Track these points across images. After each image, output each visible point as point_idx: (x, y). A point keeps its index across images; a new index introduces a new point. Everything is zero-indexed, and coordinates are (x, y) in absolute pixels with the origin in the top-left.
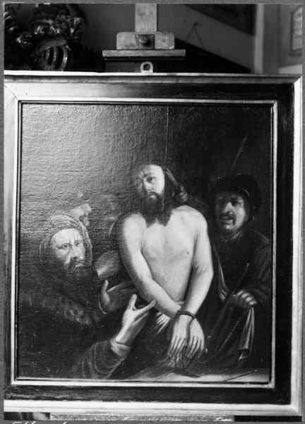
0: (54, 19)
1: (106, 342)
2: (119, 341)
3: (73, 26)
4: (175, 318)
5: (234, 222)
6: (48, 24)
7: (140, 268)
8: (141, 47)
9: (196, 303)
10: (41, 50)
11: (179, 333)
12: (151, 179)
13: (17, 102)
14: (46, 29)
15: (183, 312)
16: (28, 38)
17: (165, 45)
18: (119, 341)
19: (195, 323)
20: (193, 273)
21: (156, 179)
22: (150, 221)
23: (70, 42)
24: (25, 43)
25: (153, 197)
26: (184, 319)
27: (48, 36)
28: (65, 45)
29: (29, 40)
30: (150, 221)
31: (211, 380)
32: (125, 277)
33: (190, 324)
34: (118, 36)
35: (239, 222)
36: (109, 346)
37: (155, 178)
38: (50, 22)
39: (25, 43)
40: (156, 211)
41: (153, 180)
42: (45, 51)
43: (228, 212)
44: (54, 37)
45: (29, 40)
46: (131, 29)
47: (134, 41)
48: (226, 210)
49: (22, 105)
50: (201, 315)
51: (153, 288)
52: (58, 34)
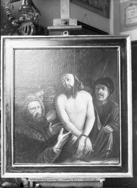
0: (27, 14)
1: (51, 148)
2: (57, 148)
3: (35, 16)
4: (79, 138)
5: (103, 97)
6: (25, 16)
7: (65, 117)
8: (63, 25)
10: (22, 27)
12: (69, 80)
14: (24, 18)
16: (17, 22)
17: (73, 24)
18: (57, 148)
23: (34, 24)
24: (15, 24)
26: (83, 138)
27: (24, 21)
28: (32, 25)
29: (17, 23)
34: (54, 20)
38: (26, 15)
39: (15, 24)
40: (71, 93)
41: (69, 80)
42: (24, 27)
43: (101, 93)
44: (27, 21)
45: (17, 23)
46: (59, 17)
47: (60, 22)
50: (91, 136)
51: (70, 125)
52: (29, 20)
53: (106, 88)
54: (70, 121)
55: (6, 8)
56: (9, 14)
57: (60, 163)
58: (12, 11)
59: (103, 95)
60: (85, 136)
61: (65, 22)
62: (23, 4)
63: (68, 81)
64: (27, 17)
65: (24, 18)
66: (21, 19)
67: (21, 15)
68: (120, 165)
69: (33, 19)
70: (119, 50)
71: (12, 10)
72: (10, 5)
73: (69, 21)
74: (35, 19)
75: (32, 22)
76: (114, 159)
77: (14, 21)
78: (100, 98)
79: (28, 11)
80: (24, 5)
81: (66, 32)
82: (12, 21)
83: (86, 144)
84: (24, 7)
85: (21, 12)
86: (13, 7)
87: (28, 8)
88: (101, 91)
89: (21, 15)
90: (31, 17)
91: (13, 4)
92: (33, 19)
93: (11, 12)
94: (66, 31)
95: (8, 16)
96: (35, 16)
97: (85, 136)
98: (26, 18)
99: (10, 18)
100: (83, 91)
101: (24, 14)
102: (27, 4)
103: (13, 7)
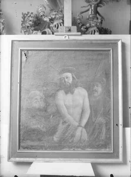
0: (93, 21)
1: (51, 137)
2: (56, 138)
3: (98, 23)
4: (76, 129)
5: (98, 93)
6: (91, 23)
7: (64, 110)
9: (85, 121)
11: (78, 133)
12: (68, 77)
13: (20, 50)
14: (90, 25)
15: (80, 126)
18: (56, 138)
19: (84, 130)
20: (83, 112)
21: (69, 77)
22: (66, 93)
23: (98, 28)
25: (68, 84)
26: (80, 129)
27: (90, 27)
28: (96, 29)
29: (85, 28)
30: (66, 93)
31: (89, 151)
32: (58, 113)
33: (82, 130)
35: (99, 93)
36: (53, 139)
37: (69, 77)
38: (92, 22)
40: (69, 90)
41: (68, 78)
42: (90, 31)
43: (95, 89)
44: (93, 27)
45: (85, 28)
48: (94, 89)
49: (22, 51)
50: (86, 127)
51: (68, 117)
52: (94, 26)
53: (100, 85)
54: (69, 114)
55: (77, 18)
56: (79, 22)
57: (62, 149)
58: (82, 20)
59: (96, 91)
60: (82, 127)
61: (68, 29)
62: (90, 13)
63: (67, 79)
64: (93, 24)
65: (90, 25)
66: (88, 25)
67: (88, 22)
68: (112, 152)
69: (97, 25)
70: (111, 51)
71: (82, 19)
72: (80, 15)
73: (71, 28)
74: (98, 24)
75: (96, 26)
76: (61, 159)
77: (83, 27)
78: (95, 94)
79: (93, 19)
80: (90, 15)
81: (66, 36)
82: (81, 27)
83: (81, 134)
84: (91, 16)
85: (88, 20)
86: (82, 17)
87: (94, 17)
88: (96, 88)
89: (88, 22)
90: (96, 23)
91: (82, 14)
92: (97, 25)
93: (81, 20)
94: (65, 36)
95: (79, 23)
96: (98, 23)
97: (82, 127)
98: (92, 24)
99: (80, 25)
100: (80, 87)
101: (91, 21)
102: (93, 13)
103: (82, 17)
